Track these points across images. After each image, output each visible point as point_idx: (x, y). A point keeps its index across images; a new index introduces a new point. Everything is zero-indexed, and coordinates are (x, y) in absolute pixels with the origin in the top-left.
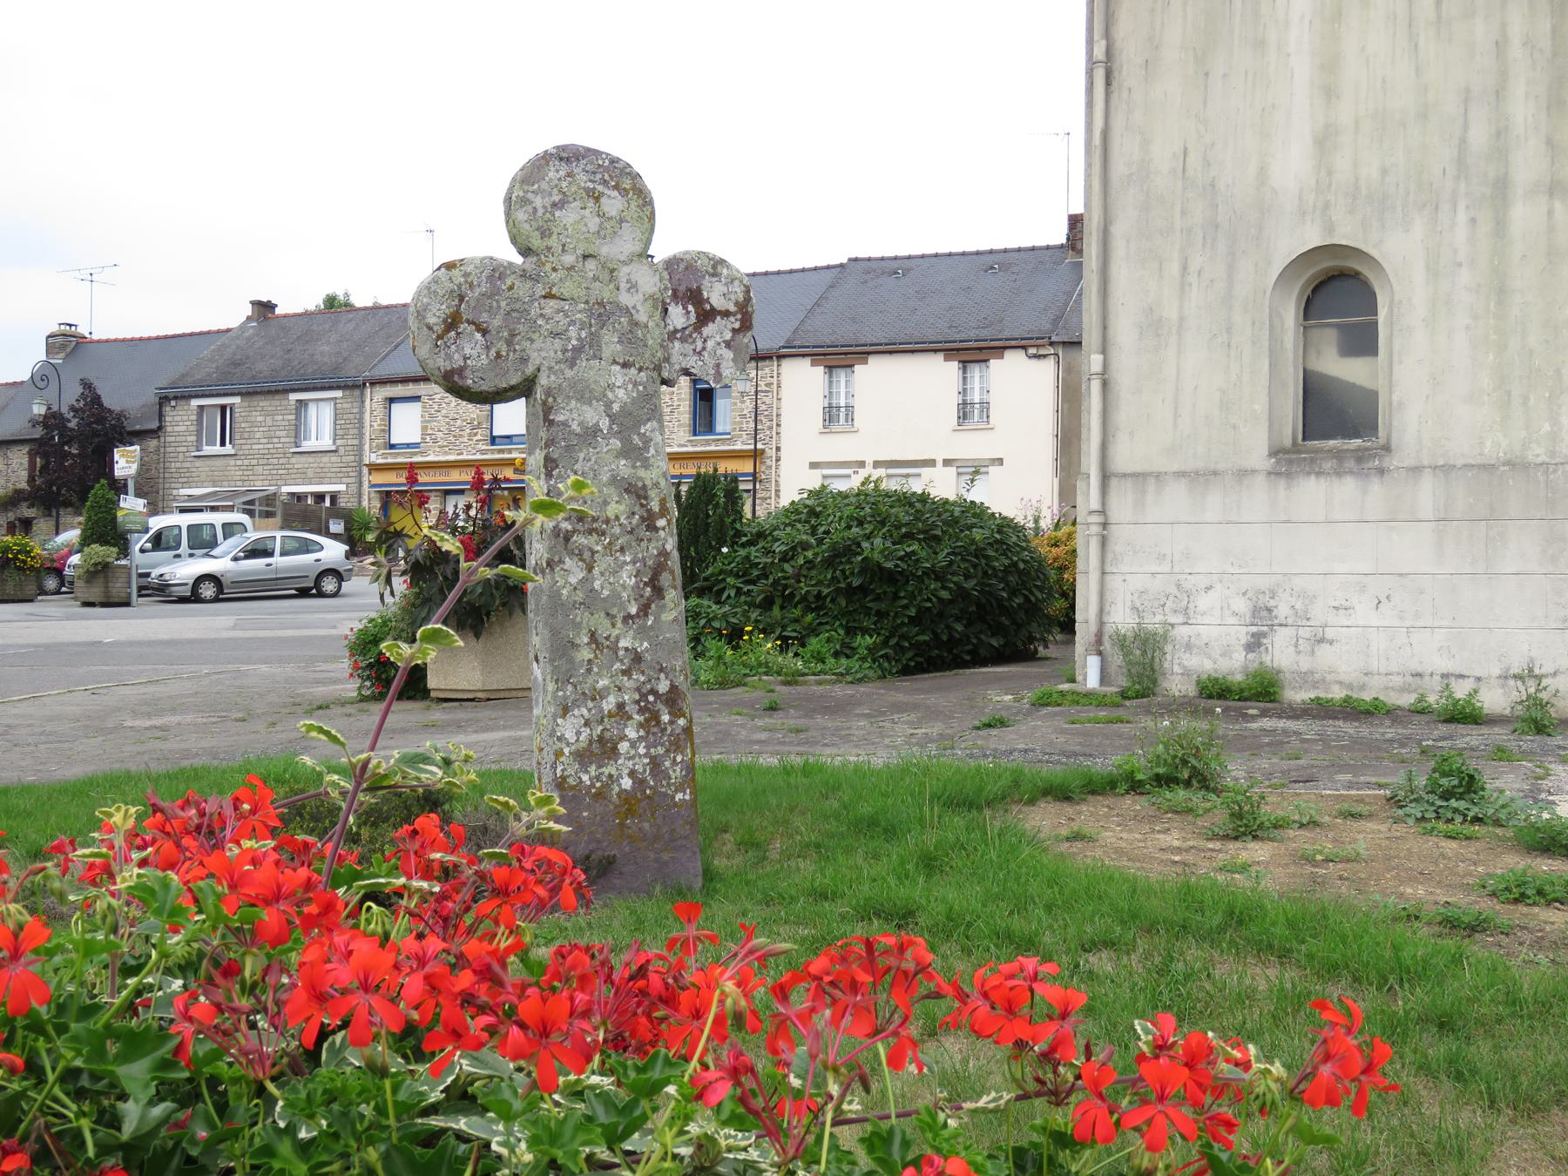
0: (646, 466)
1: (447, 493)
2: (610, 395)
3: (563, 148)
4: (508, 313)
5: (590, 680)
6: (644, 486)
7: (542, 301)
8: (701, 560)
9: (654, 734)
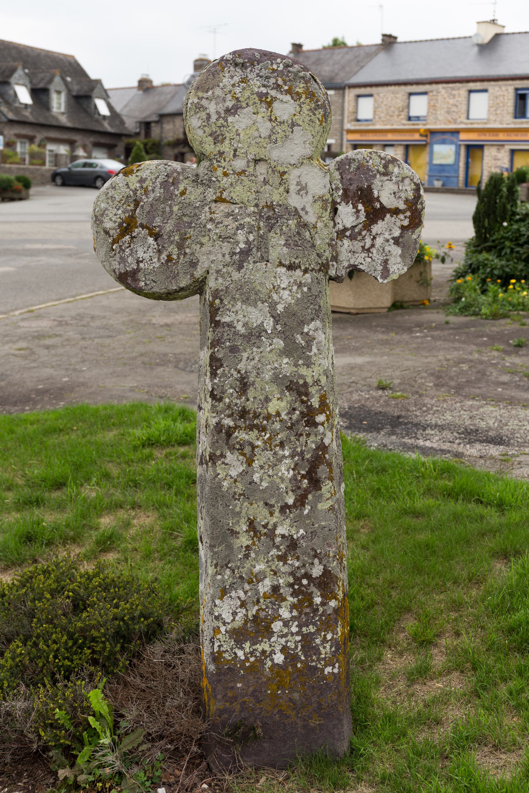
0: (308, 364)
1: (385, 146)
2: (275, 297)
3: (237, 53)
4: (180, 218)
5: (247, 565)
6: (306, 384)
7: (214, 205)
8: (490, 230)
9: (306, 614)
